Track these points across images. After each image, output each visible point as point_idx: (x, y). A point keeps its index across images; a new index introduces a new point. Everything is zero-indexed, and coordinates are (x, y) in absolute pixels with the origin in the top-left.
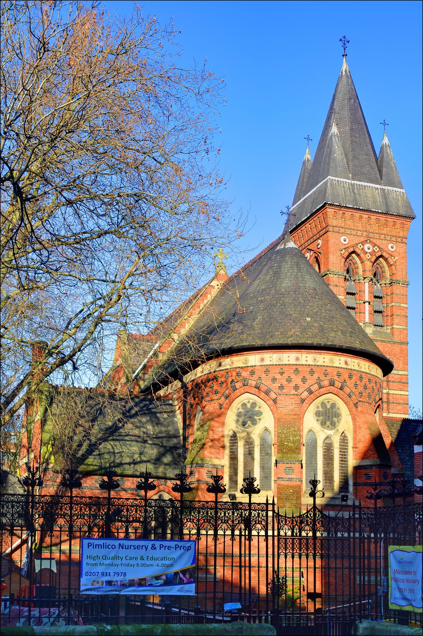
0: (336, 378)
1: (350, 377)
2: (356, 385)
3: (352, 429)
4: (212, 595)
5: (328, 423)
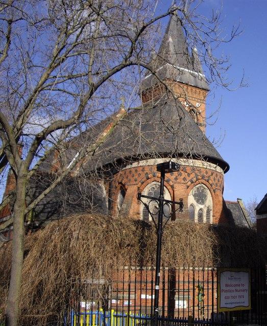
0: (205, 174)
1: (212, 174)
2: (214, 179)
3: (212, 205)
4: (139, 308)
5: (200, 201)
